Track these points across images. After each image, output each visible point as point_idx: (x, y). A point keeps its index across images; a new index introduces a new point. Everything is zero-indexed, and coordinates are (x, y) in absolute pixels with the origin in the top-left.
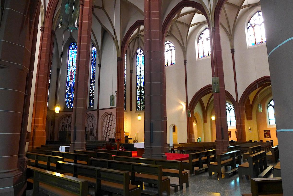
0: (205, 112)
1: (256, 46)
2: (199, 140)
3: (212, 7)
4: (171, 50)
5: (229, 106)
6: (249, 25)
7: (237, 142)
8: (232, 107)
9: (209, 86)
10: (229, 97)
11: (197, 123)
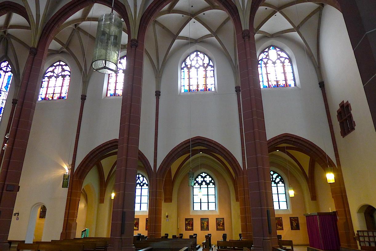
0: (103, 185)
1: (189, 93)
2: (84, 234)
3: (138, 12)
4: (64, 76)
5: (141, 179)
6: (183, 65)
7: (146, 237)
8: (145, 181)
9: (115, 141)
10: (143, 164)
11: (87, 203)
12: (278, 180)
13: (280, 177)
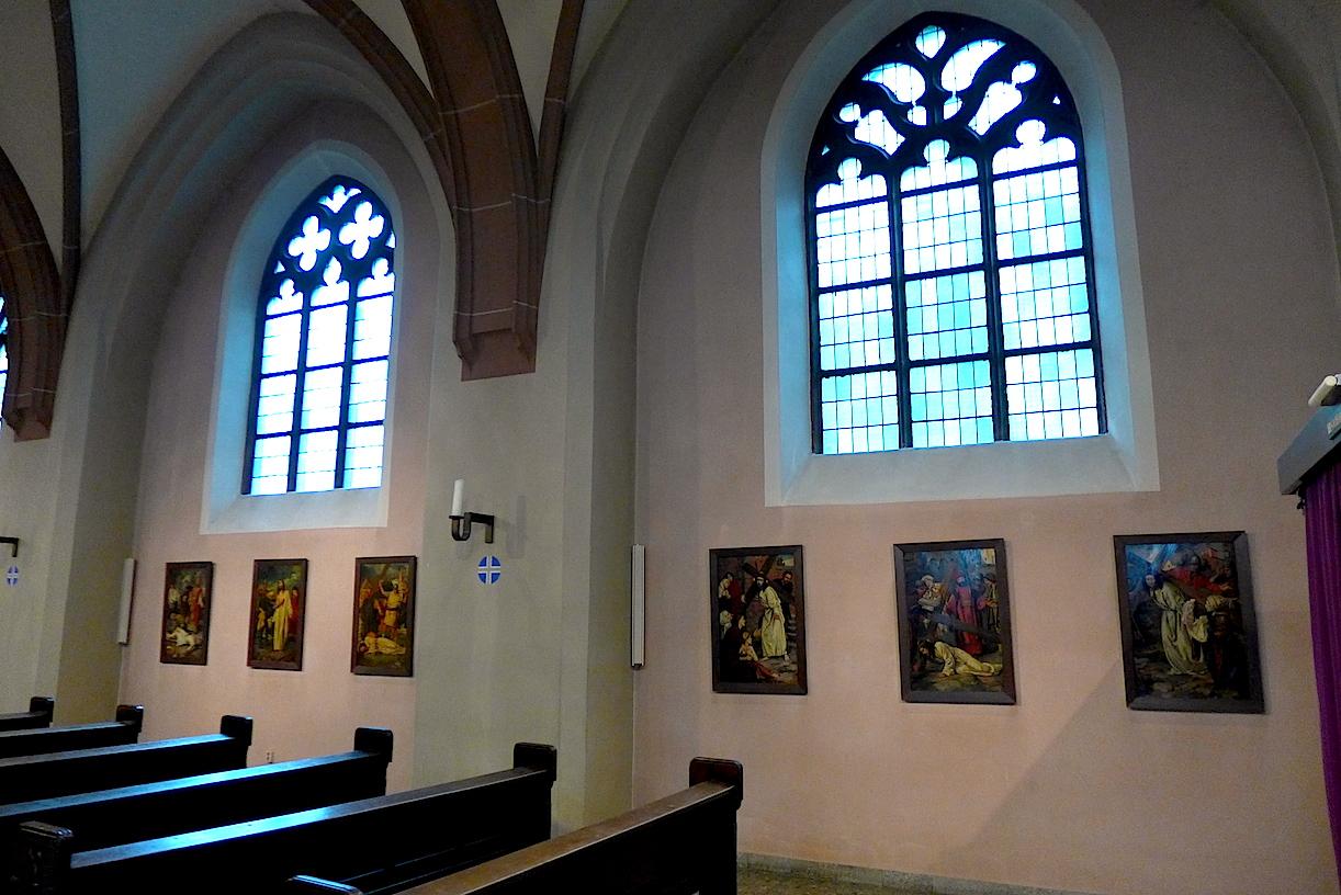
12: (1001, 99)
13: (1025, 72)
